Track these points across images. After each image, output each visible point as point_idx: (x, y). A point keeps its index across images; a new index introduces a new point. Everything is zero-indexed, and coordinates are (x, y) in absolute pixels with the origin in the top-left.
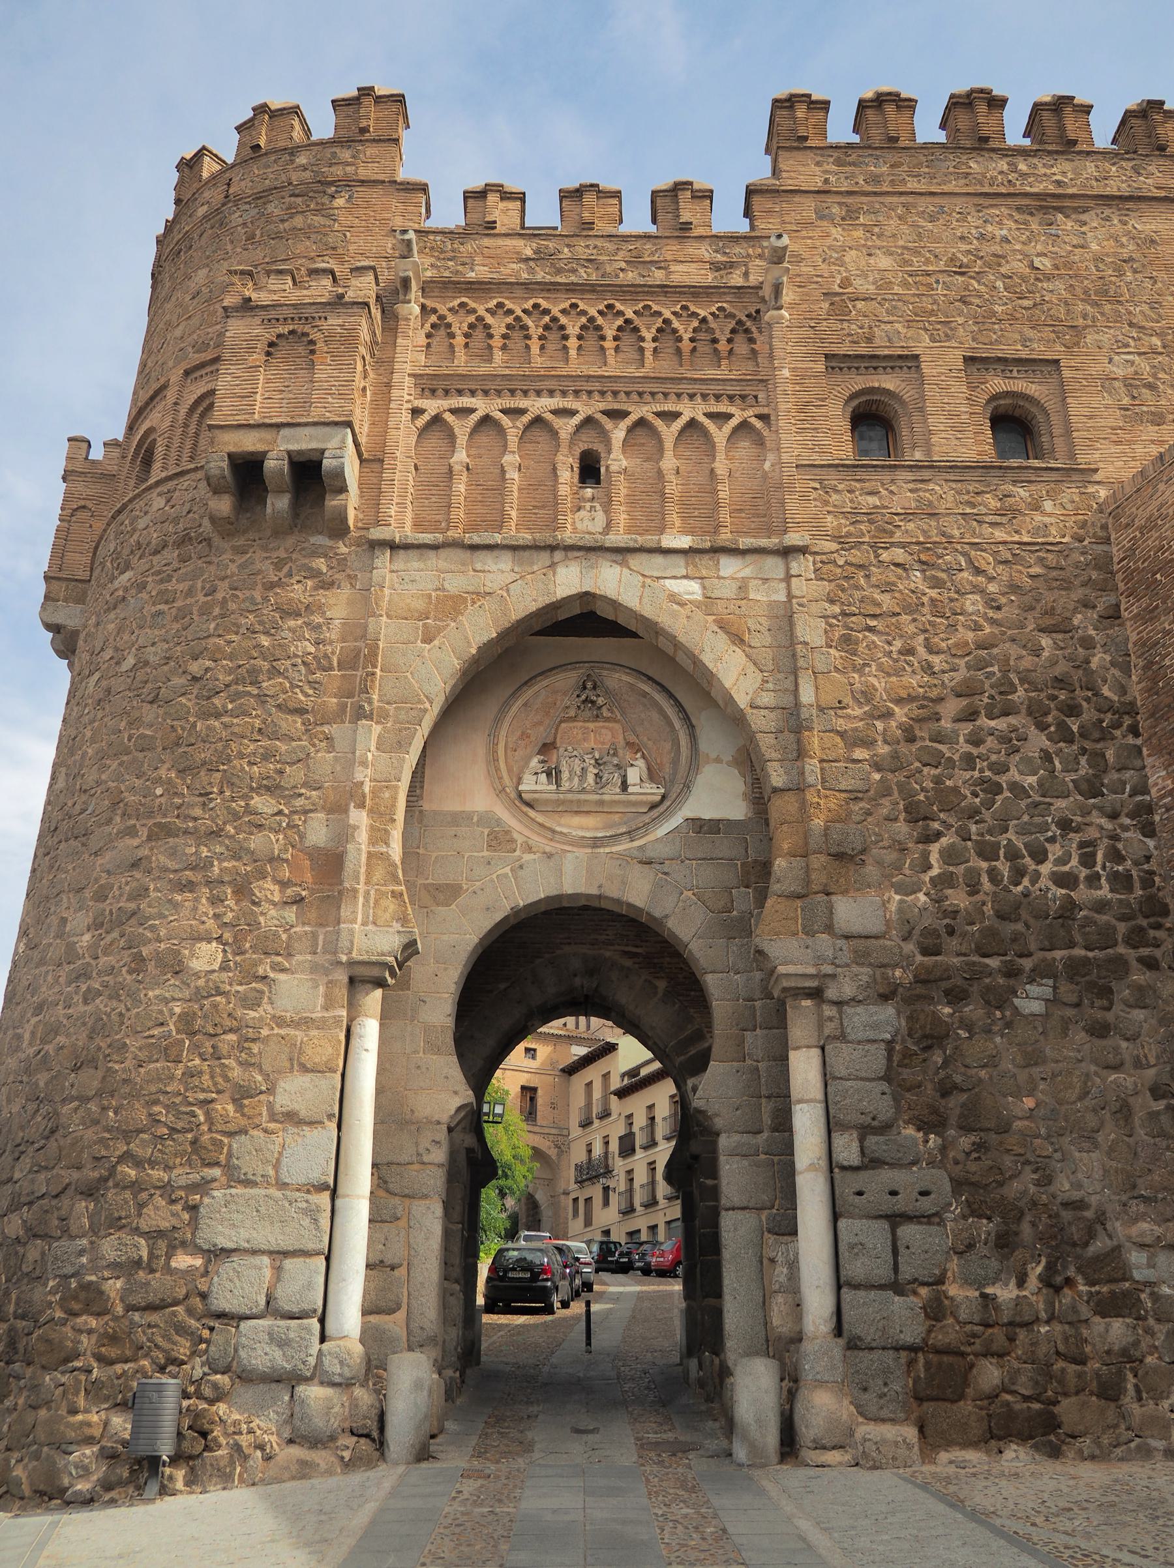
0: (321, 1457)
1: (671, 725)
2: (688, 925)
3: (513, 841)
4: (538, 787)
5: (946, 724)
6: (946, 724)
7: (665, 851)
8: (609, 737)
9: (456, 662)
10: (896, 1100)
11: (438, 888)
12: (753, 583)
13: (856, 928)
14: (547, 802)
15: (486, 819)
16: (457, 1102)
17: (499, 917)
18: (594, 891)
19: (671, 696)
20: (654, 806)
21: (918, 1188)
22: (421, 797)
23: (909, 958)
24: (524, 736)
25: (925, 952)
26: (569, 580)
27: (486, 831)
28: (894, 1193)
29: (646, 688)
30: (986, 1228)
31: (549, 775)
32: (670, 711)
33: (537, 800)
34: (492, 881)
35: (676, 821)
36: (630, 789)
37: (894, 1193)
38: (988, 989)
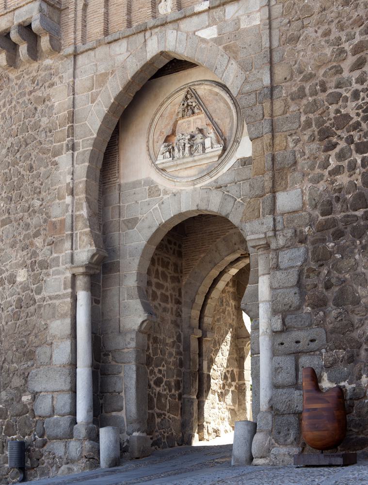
3: (159, 190)
4: (164, 161)
5: (346, 74)
7: (228, 179)
9: (105, 109)
11: (129, 221)
13: (287, 208)
14: (170, 167)
15: (149, 182)
18: (195, 208)
21: (309, 338)
25: (323, 214)
26: (153, 47)
27: (147, 188)
28: (298, 342)
30: (342, 353)
34: (151, 212)
35: (232, 162)
37: (298, 342)
38: (354, 228)
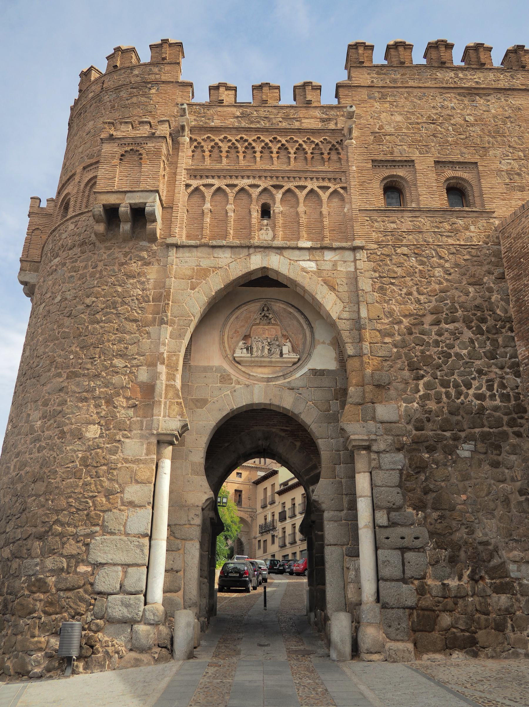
0: (145, 657)
1: (302, 327)
2: (310, 417)
3: (231, 379)
4: (243, 355)
5: (426, 326)
6: (426, 326)
7: (300, 384)
8: (274, 332)
9: (206, 298)
10: (404, 496)
11: (197, 400)
12: (339, 263)
13: (386, 418)
14: (246, 362)
15: (219, 369)
16: (206, 497)
17: (225, 413)
18: (268, 402)
19: (302, 314)
20: (294, 364)
21: (414, 536)
22: (190, 359)
23: (410, 432)
24: (236, 332)
25: (417, 429)
26: (256, 262)
27: (219, 375)
28: (403, 538)
29: (291, 310)
30: (444, 554)
31: (247, 349)
32: (302, 321)
33: (242, 361)
34: (222, 397)
35: (305, 370)
36: (284, 356)
37: (403, 538)
38: (445, 446)
